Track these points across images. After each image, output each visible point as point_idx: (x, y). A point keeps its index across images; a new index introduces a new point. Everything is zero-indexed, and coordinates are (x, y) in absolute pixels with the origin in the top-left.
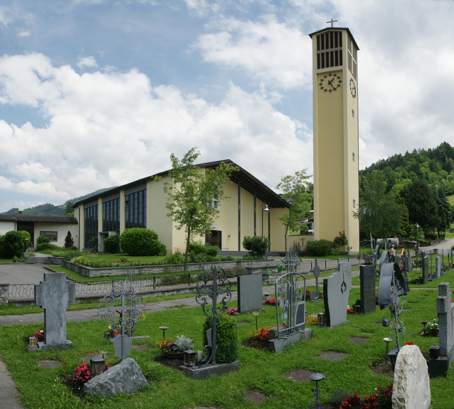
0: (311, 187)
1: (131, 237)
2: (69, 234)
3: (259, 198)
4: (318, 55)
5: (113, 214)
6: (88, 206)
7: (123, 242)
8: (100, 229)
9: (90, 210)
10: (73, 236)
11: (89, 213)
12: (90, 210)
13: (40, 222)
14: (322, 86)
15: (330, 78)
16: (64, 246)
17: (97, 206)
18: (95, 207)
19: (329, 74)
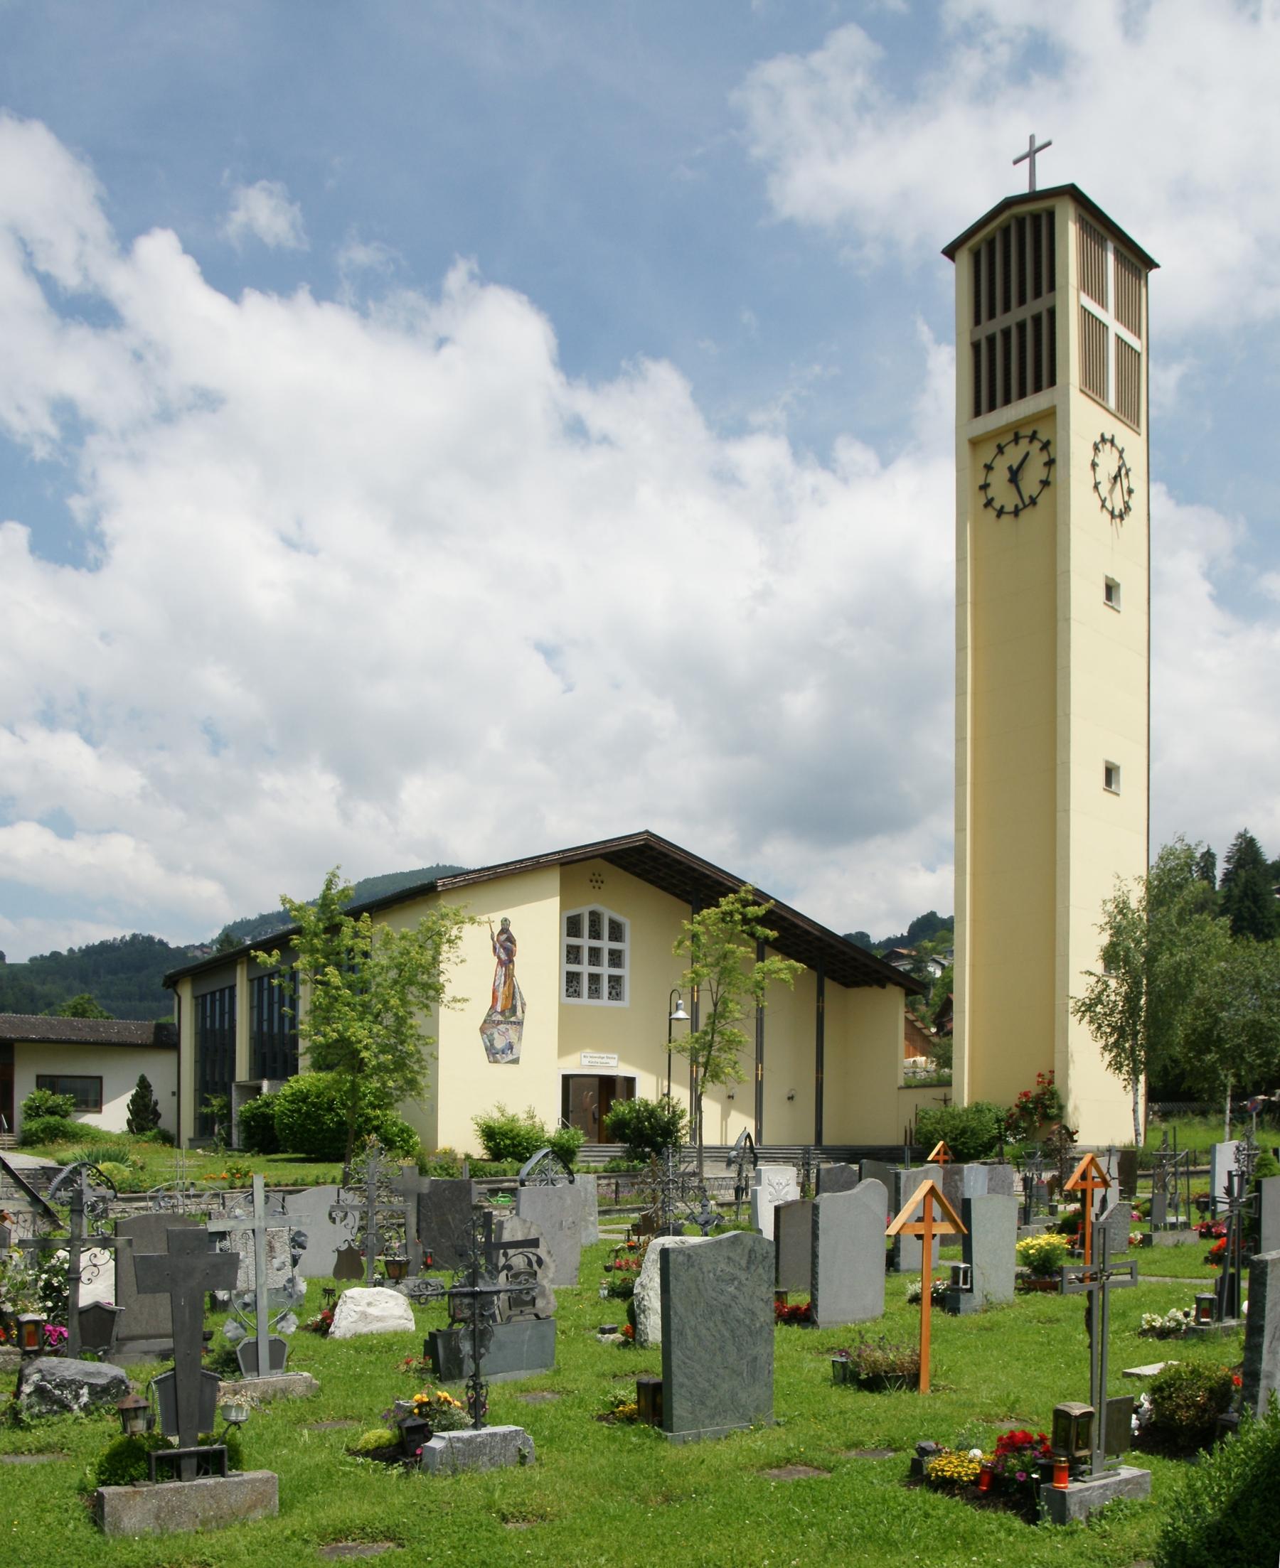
0: (931, 929)
1: (304, 1100)
2: (144, 1085)
3: (834, 979)
4: (976, 347)
5: (222, 1015)
6: (206, 988)
7: (1221, 1125)
8: (242, 1072)
9: (213, 1003)
10: (161, 1093)
11: (265, 1017)
12: (213, 1003)
13: (33, 1041)
14: (997, 505)
15: (1013, 455)
16: (125, 1127)
17: (232, 988)
18: (227, 992)
19: (1011, 437)
